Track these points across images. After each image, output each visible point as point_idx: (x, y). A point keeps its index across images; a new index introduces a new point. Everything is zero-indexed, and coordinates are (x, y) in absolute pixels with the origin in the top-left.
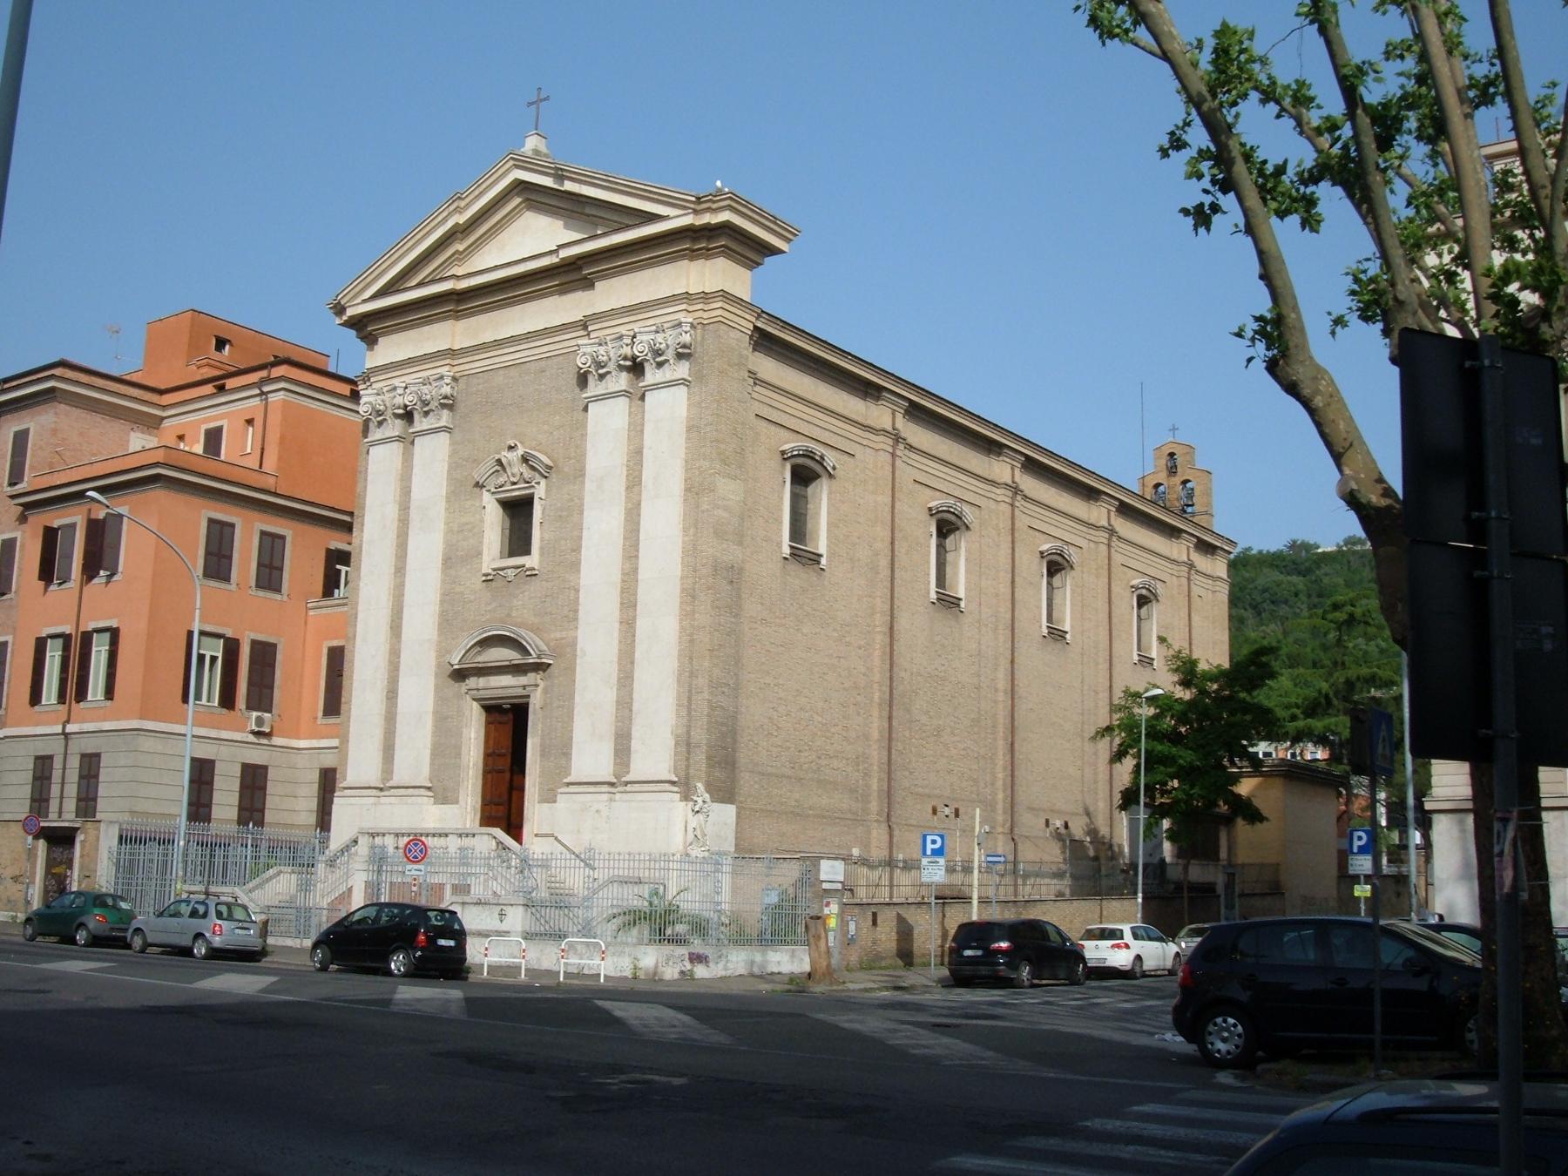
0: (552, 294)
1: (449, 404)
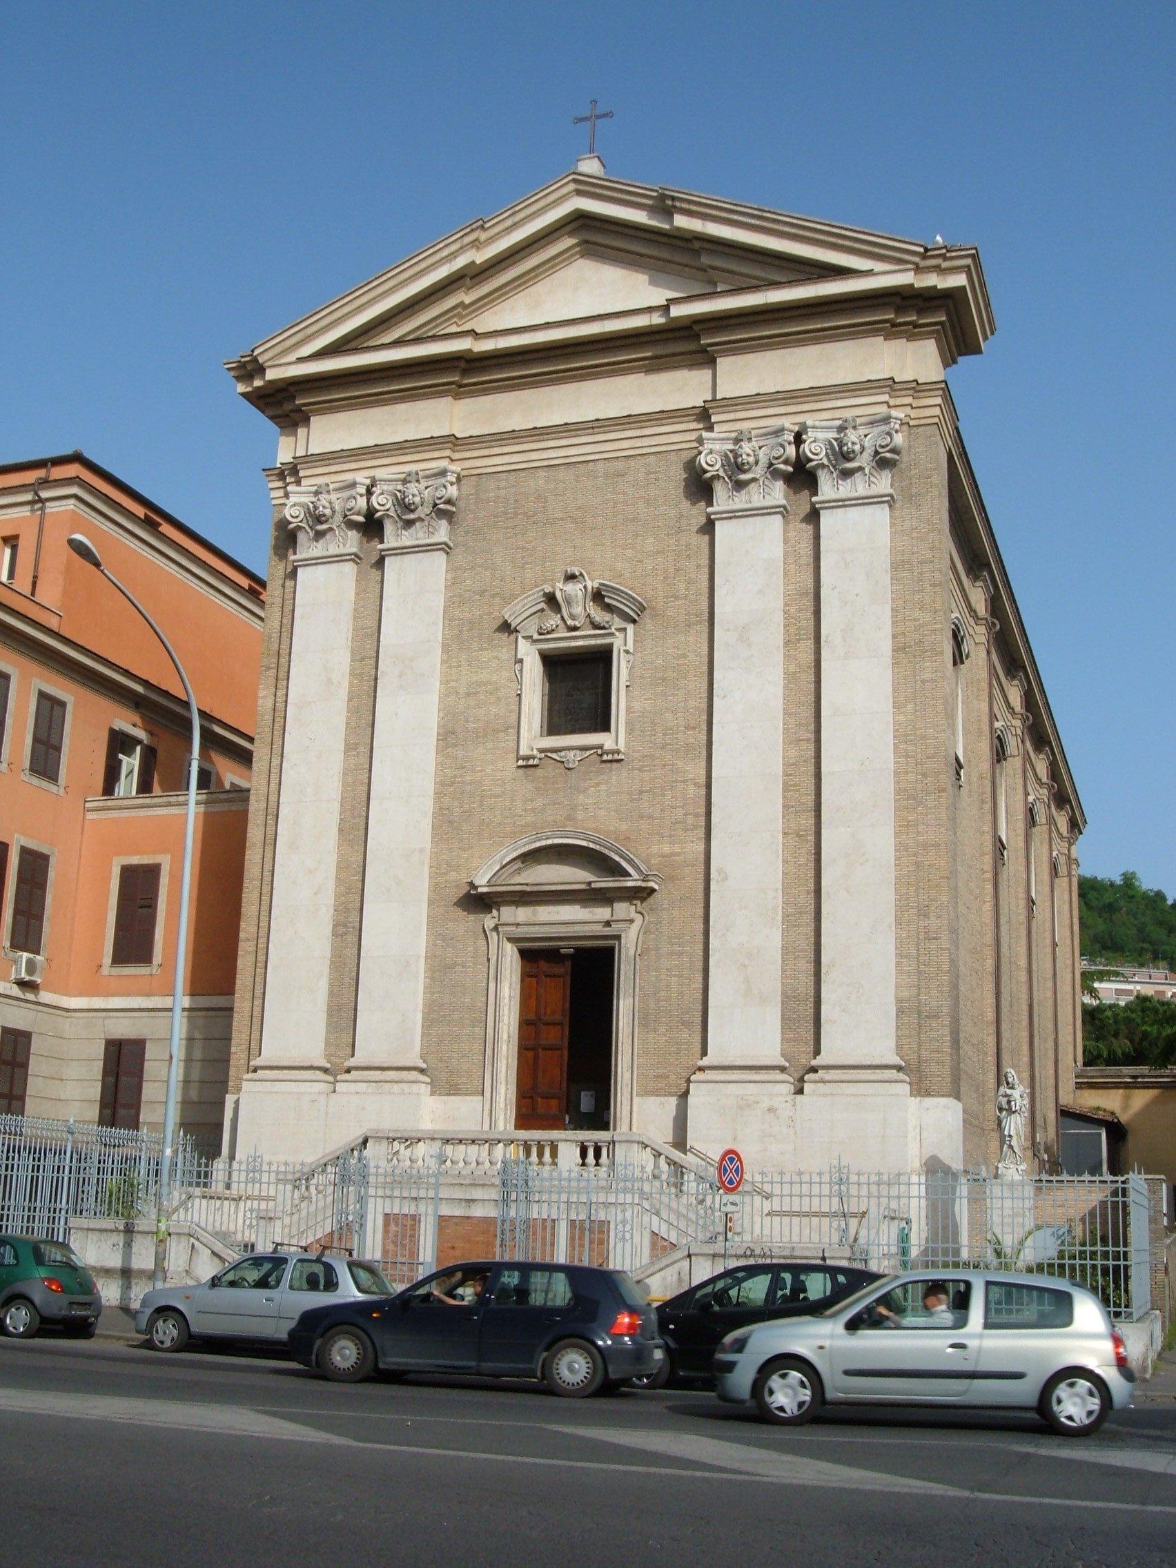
1: (444, 511)
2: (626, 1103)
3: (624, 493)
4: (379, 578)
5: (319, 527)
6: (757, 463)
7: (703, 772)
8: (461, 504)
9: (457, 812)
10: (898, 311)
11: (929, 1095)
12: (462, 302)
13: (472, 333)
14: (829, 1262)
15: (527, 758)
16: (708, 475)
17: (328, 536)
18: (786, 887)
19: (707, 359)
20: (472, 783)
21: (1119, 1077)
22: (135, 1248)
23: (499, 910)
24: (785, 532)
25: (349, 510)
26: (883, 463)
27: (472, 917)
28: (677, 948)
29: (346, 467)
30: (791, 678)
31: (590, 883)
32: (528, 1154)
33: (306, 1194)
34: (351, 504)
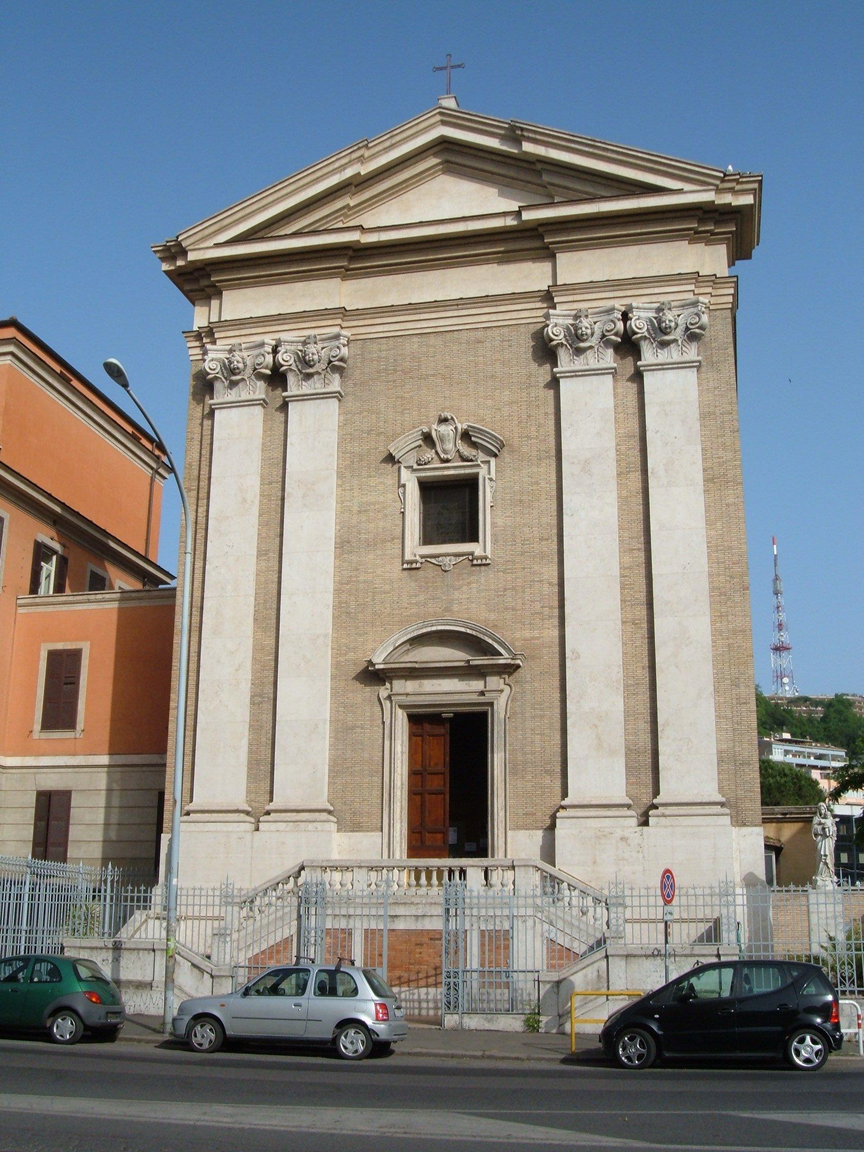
0: (487, 262)
1: (336, 367)
2: (502, 836)
3: (484, 356)
4: (283, 419)
5: (234, 378)
6: (592, 334)
7: (556, 574)
8: (350, 362)
9: (353, 605)
10: (699, 222)
11: (744, 825)
12: (348, 204)
13: (360, 228)
14: (723, 959)
15: (411, 562)
16: (554, 343)
17: (241, 385)
18: (625, 664)
19: (549, 254)
20: (365, 582)
21: (773, 814)
22: (123, 963)
23: (391, 683)
24: (615, 388)
25: (259, 365)
26: (692, 337)
27: (368, 689)
28: (538, 712)
29: (254, 331)
30: (623, 502)
31: (468, 661)
32: (418, 878)
33: (251, 914)
34: (261, 360)
